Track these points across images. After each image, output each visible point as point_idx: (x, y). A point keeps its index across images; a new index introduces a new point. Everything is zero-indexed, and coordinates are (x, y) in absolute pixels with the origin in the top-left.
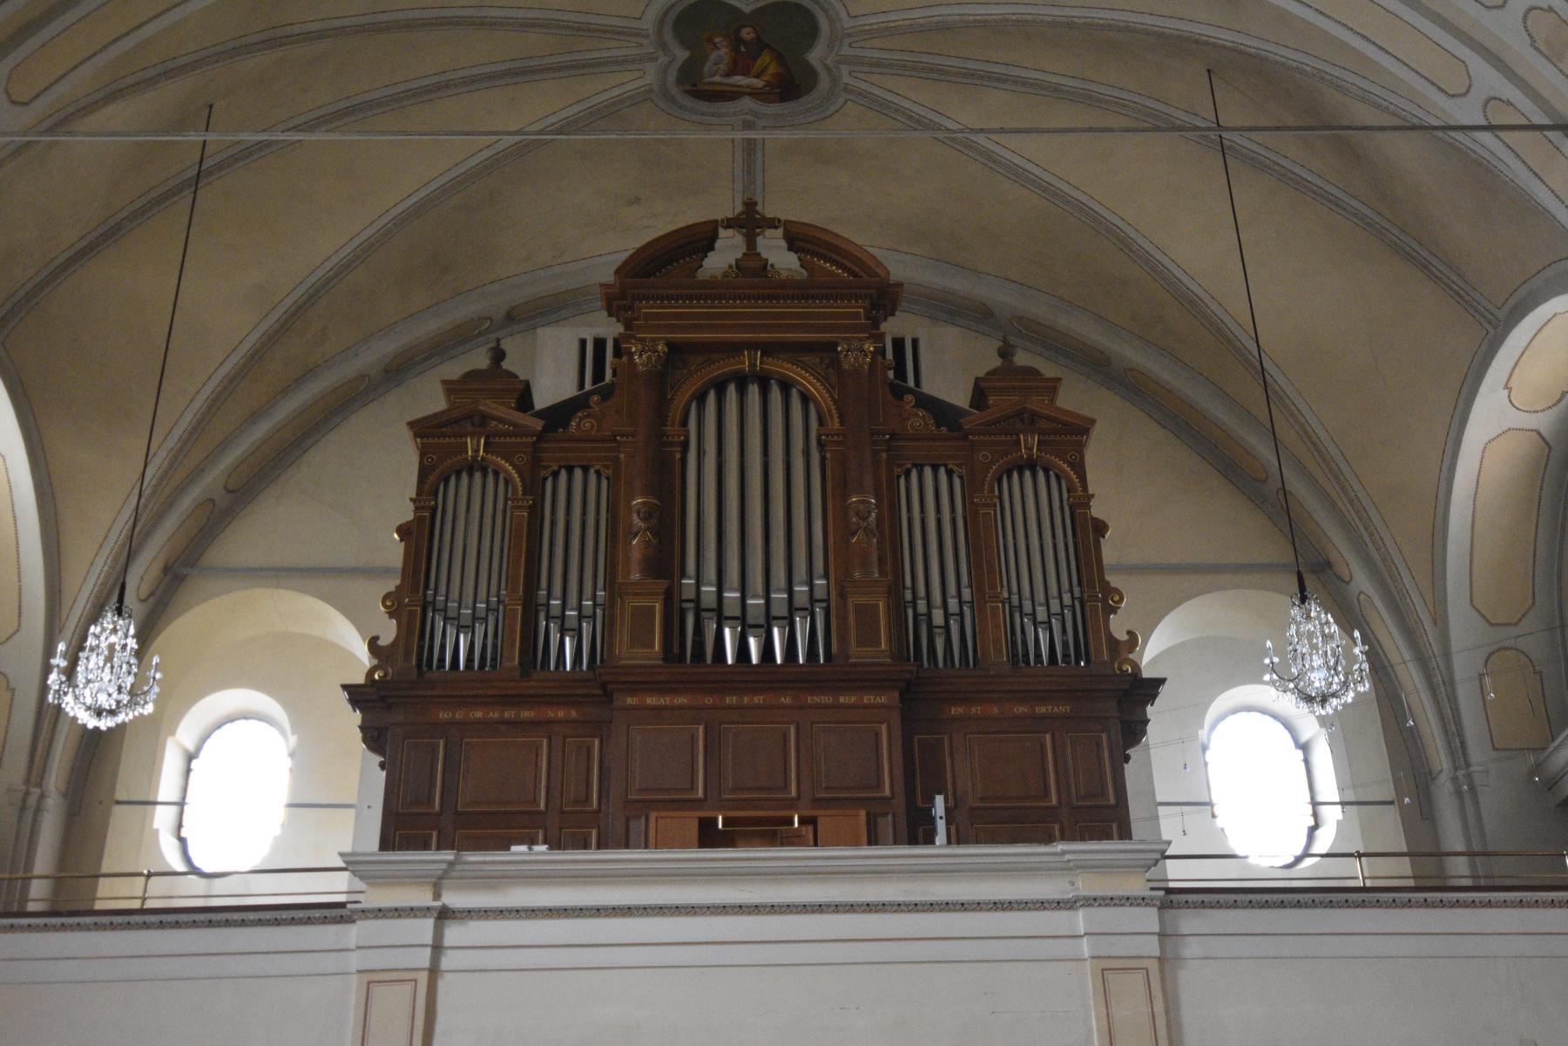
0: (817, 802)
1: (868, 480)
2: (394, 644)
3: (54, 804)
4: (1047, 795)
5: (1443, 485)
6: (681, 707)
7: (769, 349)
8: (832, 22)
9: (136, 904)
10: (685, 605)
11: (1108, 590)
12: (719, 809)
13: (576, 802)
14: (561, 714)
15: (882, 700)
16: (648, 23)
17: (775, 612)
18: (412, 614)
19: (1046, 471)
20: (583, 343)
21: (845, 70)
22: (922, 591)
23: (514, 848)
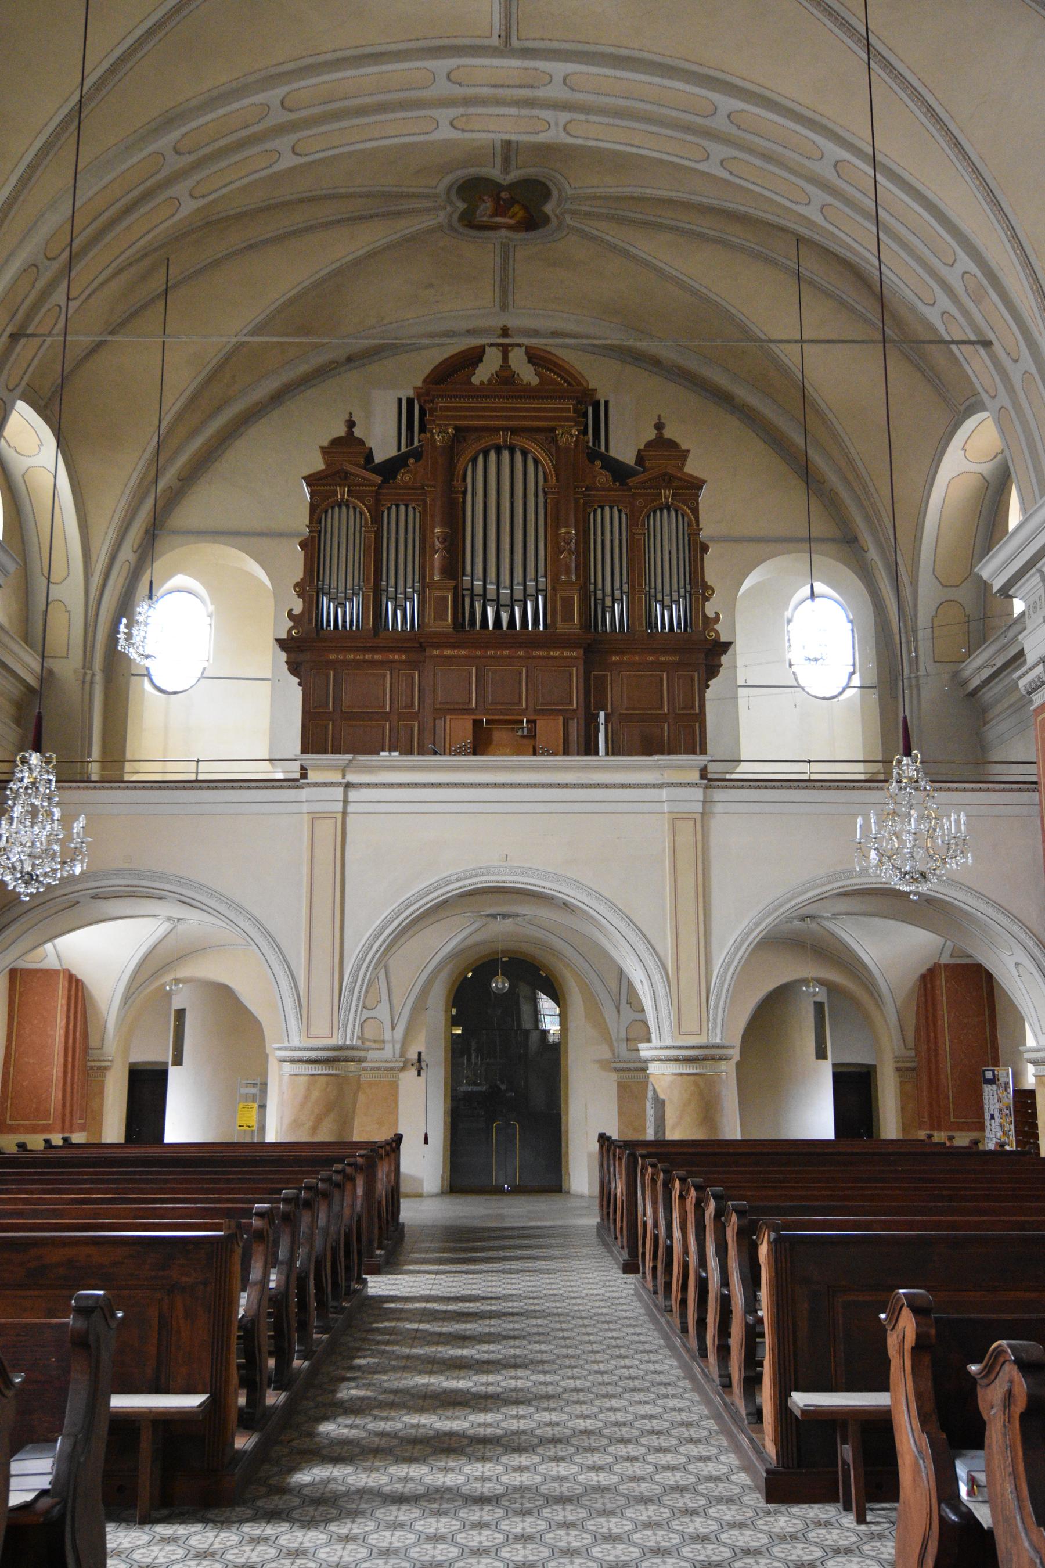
0: (537, 711)
1: (572, 520)
2: (302, 613)
3: (99, 678)
4: (662, 707)
5: (924, 499)
6: (464, 657)
7: (515, 431)
8: (559, 190)
9: (193, 777)
10: (465, 592)
11: (706, 587)
12: (484, 715)
13: (406, 707)
14: (396, 657)
15: (574, 654)
16: (441, 189)
17: (516, 597)
18: (311, 596)
19: (676, 511)
20: (400, 400)
21: (568, 218)
22: (600, 586)
23: (382, 754)
